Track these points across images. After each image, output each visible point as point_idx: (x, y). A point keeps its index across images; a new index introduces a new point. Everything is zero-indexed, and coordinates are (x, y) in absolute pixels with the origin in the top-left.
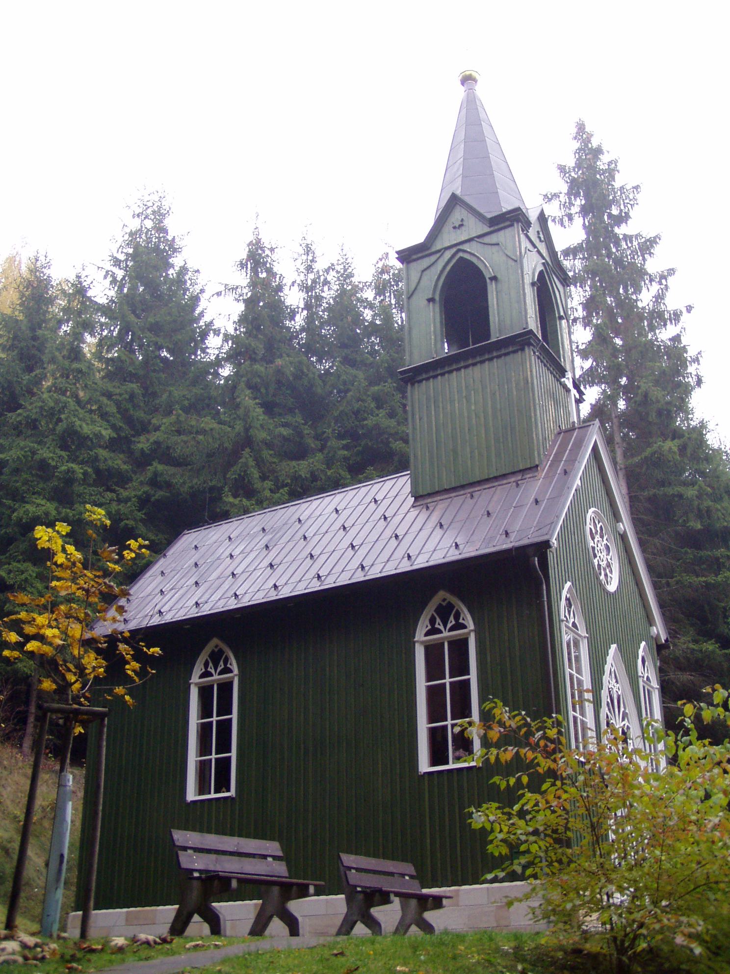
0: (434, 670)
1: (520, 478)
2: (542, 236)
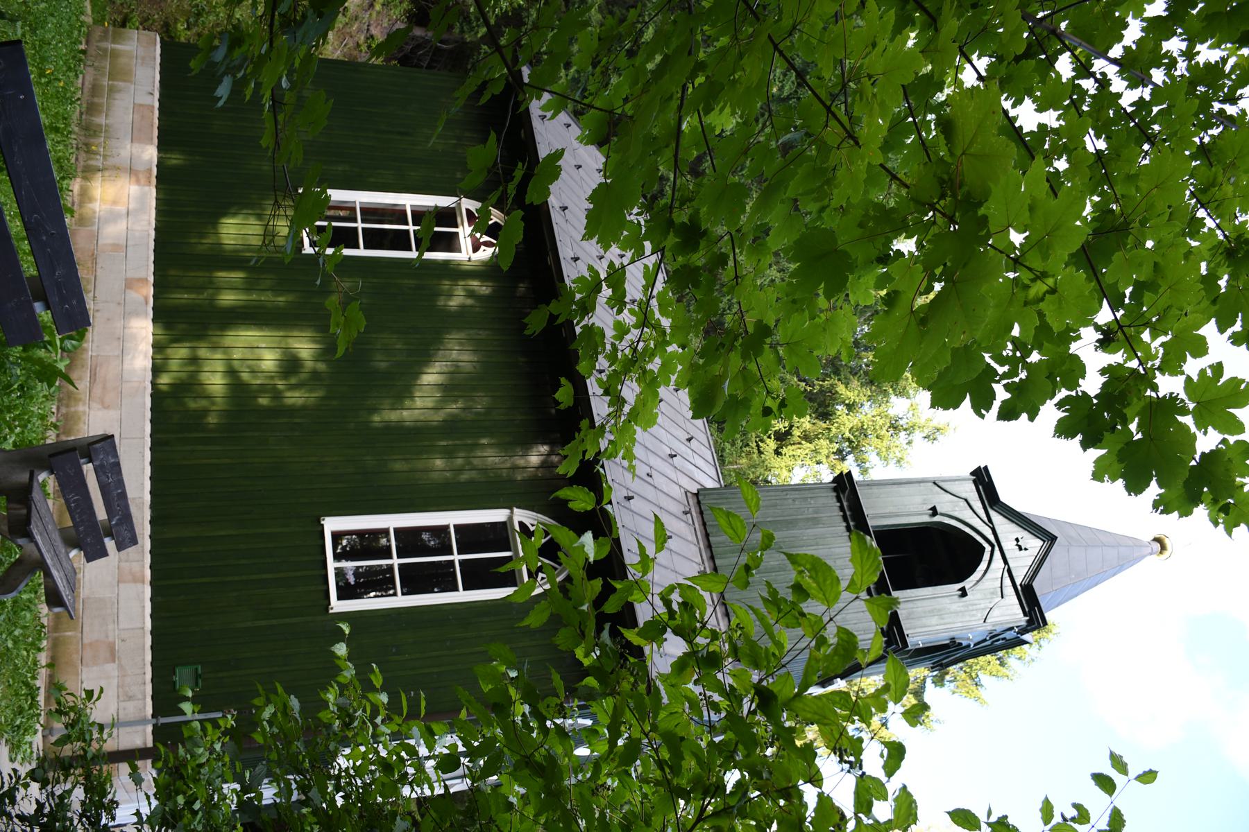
0: (471, 537)
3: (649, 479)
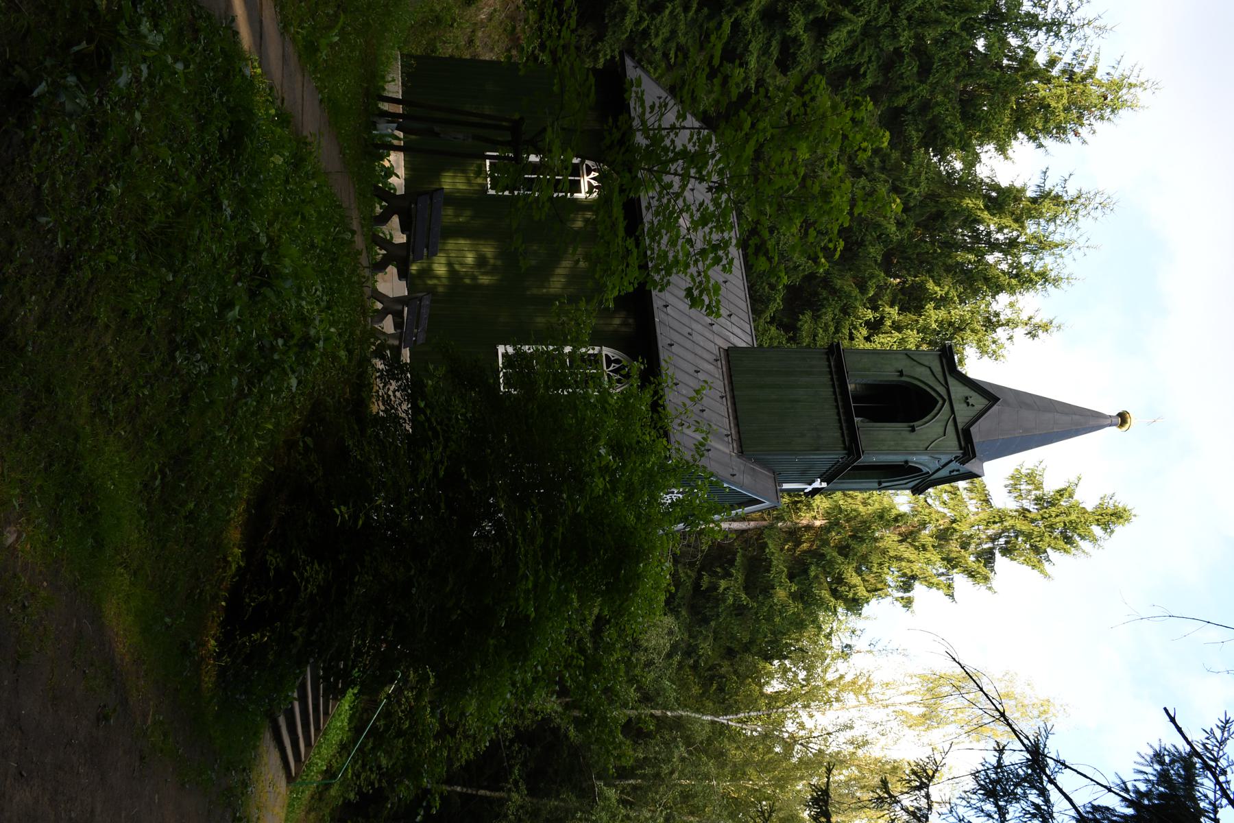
1: (734, 437)
2: (955, 473)
3: (690, 337)
